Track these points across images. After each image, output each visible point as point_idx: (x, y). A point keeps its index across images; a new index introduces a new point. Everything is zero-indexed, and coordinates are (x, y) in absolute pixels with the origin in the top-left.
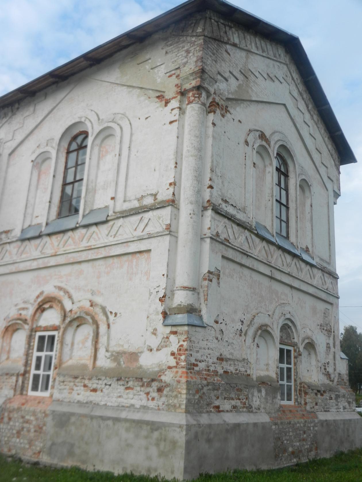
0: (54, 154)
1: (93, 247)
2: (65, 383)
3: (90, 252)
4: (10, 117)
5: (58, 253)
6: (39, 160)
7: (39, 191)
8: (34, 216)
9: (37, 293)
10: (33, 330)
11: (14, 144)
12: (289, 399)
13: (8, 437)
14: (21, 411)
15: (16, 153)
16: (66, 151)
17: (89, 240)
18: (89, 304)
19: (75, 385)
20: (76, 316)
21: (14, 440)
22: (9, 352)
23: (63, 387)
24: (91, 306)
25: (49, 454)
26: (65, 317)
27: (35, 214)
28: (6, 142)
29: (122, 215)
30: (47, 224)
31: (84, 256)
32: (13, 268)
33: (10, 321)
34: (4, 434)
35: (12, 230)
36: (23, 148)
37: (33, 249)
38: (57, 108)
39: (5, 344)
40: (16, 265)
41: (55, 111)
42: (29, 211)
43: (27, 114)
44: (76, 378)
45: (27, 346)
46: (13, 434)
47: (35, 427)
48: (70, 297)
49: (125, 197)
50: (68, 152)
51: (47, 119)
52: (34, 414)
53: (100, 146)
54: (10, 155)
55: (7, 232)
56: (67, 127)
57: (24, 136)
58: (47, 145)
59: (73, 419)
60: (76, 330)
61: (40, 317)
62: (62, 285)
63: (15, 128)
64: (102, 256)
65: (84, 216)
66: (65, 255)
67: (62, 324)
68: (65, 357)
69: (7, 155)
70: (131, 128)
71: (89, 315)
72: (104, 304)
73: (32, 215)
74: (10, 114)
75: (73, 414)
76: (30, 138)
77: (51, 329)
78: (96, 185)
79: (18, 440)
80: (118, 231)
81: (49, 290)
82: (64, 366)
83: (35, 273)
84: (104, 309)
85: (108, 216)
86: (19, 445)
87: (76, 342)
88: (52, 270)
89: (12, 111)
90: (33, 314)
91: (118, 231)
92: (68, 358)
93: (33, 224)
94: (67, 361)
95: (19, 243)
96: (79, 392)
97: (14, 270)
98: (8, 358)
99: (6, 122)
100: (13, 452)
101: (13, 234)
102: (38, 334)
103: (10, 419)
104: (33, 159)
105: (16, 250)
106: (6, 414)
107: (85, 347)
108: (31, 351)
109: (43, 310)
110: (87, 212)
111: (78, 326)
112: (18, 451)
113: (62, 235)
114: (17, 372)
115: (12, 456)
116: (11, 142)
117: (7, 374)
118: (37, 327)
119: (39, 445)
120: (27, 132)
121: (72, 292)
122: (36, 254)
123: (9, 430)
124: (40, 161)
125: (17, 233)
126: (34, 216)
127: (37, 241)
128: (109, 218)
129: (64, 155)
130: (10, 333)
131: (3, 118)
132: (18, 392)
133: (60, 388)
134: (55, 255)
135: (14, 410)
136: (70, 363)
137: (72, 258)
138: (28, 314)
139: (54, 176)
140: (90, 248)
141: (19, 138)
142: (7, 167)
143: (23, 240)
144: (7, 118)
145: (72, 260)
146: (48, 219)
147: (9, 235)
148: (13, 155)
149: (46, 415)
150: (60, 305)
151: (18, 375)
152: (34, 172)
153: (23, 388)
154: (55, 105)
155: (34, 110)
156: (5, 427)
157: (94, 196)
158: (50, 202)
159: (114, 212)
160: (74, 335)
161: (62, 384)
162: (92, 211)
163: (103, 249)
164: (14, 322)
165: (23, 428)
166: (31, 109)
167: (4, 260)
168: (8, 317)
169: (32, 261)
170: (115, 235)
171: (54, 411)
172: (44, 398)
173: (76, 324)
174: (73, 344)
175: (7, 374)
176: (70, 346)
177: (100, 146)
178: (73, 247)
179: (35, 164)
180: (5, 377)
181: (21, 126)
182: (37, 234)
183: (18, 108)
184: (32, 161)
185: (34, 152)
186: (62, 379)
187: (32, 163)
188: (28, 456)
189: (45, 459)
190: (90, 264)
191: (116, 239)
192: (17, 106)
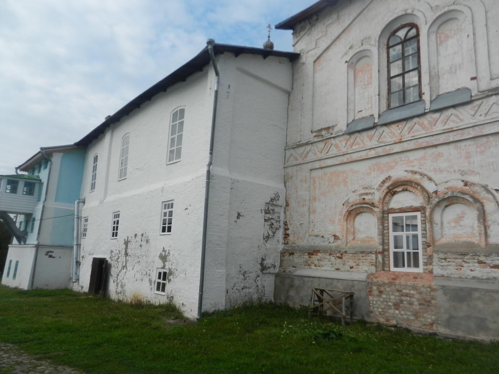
0: (375, 51)
1: (455, 129)
2: (448, 260)
3: (451, 134)
4: (309, 29)
5: (403, 140)
6: (354, 60)
7: (357, 89)
8: (356, 111)
9: (382, 178)
10: (386, 213)
11: (319, 51)
12: (416, 265)
13: (382, 309)
14: (395, 285)
15: (322, 59)
16: (386, 47)
17: (445, 123)
18: (462, 184)
19: (464, 261)
20: (446, 197)
21: (391, 311)
22: (354, 233)
23: (445, 264)
24: (466, 185)
25: (448, 324)
26: (429, 197)
27: (358, 109)
28: (308, 52)
29: (494, 93)
30: (379, 116)
31: (442, 139)
32: (344, 159)
33: (352, 206)
34: (376, 306)
35: (333, 127)
36: (330, 53)
37: (366, 141)
38: (367, 9)
39: (349, 226)
40: (348, 156)
41: (365, 12)
42: (351, 107)
43: (330, 21)
44: (465, 255)
45: (381, 227)
46: (389, 306)
47: (418, 300)
48: (430, 179)
49: (491, 75)
50: (388, 48)
51: (356, 21)
52: (414, 288)
53: (437, 32)
54: (315, 62)
55: (328, 128)
56: (387, 23)
57: (329, 42)
58: (362, 44)
59: (476, 295)
60: (444, 210)
61: (390, 200)
62: (415, 169)
63: (317, 38)
64: (470, 136)
65: (431, 102)
66: (415, 141)
67: (428, 205)
68: (437, 236)
69: (312, 63)
70: (471, 11)
71: (466, 194)
72: (484, 183)
73: (354, 110)
74: (308, 27)
75: (476, 290)
76: (337, 42)
77: (397, 211)
78: (438, 71)
79: (397, 312)
80: (490, 109)
81: (399, 173)
82: (437, 244)
83: (374, 161)
84: (485, 188)
85: (471, 96)
86: (399, 316)
87: (445, 221)
88: (396, 157)
89: (310, 23)
90: (382, 198)
91: (490, 109)
92: (440, 236)
93: (357, 118)
94: (440, 239)
95: (347, 137)
96: (472, 268)
97: (345, 161)
98: (354, 239)
99: (304, 35)
100: (394, 322)
101: (336, 129)
102: (391, 216)
103: (381, 292)
104: (348, 60)
105: (344, 143)
106: (375, 288)
107: (460, 226)
108: (385, 232)
109: (395, 193)
110: (434, 98)
111: (446, 206)
112: (400, 322)
113: (404, 123)
114: (375, 250)
115: (395, 326)
116: (316, 50)
117: (362, 252)
118: (388, 209)
119: (429, 318)
120: (333, 38)
121: (431, 174)
122: (374, 143)
123: (383, 302)
124: (356, 61)
125: (342, 126)
126: (356, 111)
127: (372, 132)
128: (473, 99)
129: (385, 51)
130: (353, 216)
131: (300, 31)
132: (380, 268)
133: (442, 264)
134: (400, 142)
135: (384, 284)
136: (444, 241)
137: (423, 142)
138: (377, 197)
139: (379, 71)
140: (450, 130)
141: (323, 45)
142: (314, 73)
143: (351, 134)
144: (306, 31)
145: (424, 145)
146: (379, 111)
147: (331, 131)
148: (318, 61)
149: (433, 290)
150: (419, 187)
151: (376, 253)
152: (349, 71)
153: (385, 265)
154: (364, 7)
155: (338, 17)
156: (375, 299)
157: (438, 82)
158: (379, 95)
159: (479, 92)
160: (442, 215)
161: (443, 261)
162: (438, 96)
163: (471, 129)
164: (358, 206)
165: (402, 301)
166: (335, 16)
167: (330, 153)
168: (347, 202)
169: (368, 151)
170: (486, 114)
171: (444, 286)
172: (418, 274)
173: (444, 204)
174: (442, 223)
175: (362, 252)
176: (439, 225)
177: (437, 32)
178: (424, 132)
179: (350, 64)
180: (361, 255)
181: (324, 34)
182: (371, 125)
183: (317, 19)
184: (346, 62)
185: (346, 54)
186: (442, 256)
187: (347, 64)
188: (416, 326)
189: (442, 330)
190: (452, 146)
191: (488, 117)
192: (315, 17)
